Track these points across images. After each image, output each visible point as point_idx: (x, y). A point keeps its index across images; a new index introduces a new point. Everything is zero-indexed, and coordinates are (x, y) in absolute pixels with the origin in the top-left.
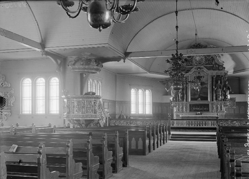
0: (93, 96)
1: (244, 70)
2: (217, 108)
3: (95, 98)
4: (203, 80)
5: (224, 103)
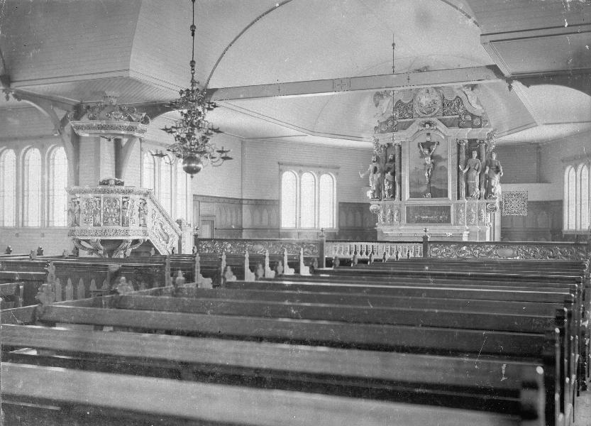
0: (117, 187)
1: (528, 126)
2: (470, 217)
3: (123, 192)
4: (437, 150)
5: (487, 204)
